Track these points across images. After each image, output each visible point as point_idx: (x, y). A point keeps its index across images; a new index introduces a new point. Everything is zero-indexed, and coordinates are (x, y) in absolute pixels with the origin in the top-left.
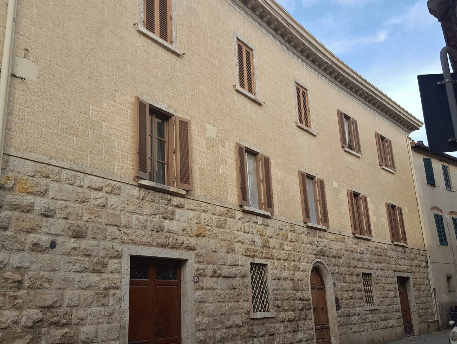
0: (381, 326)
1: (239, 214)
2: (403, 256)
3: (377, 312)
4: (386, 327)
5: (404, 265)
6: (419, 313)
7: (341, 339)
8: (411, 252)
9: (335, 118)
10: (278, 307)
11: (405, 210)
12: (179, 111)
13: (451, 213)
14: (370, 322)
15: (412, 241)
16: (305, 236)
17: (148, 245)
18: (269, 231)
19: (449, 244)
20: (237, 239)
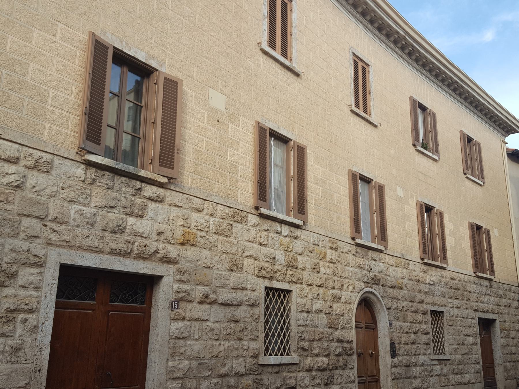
2: (489, 292)
3: (448, 362)
5: (489, 303)
6: (505, 367)
8: (499, 288)
11: (494, 234)
12: (437, 207)
14: (438, 375)
16: (351, 257)
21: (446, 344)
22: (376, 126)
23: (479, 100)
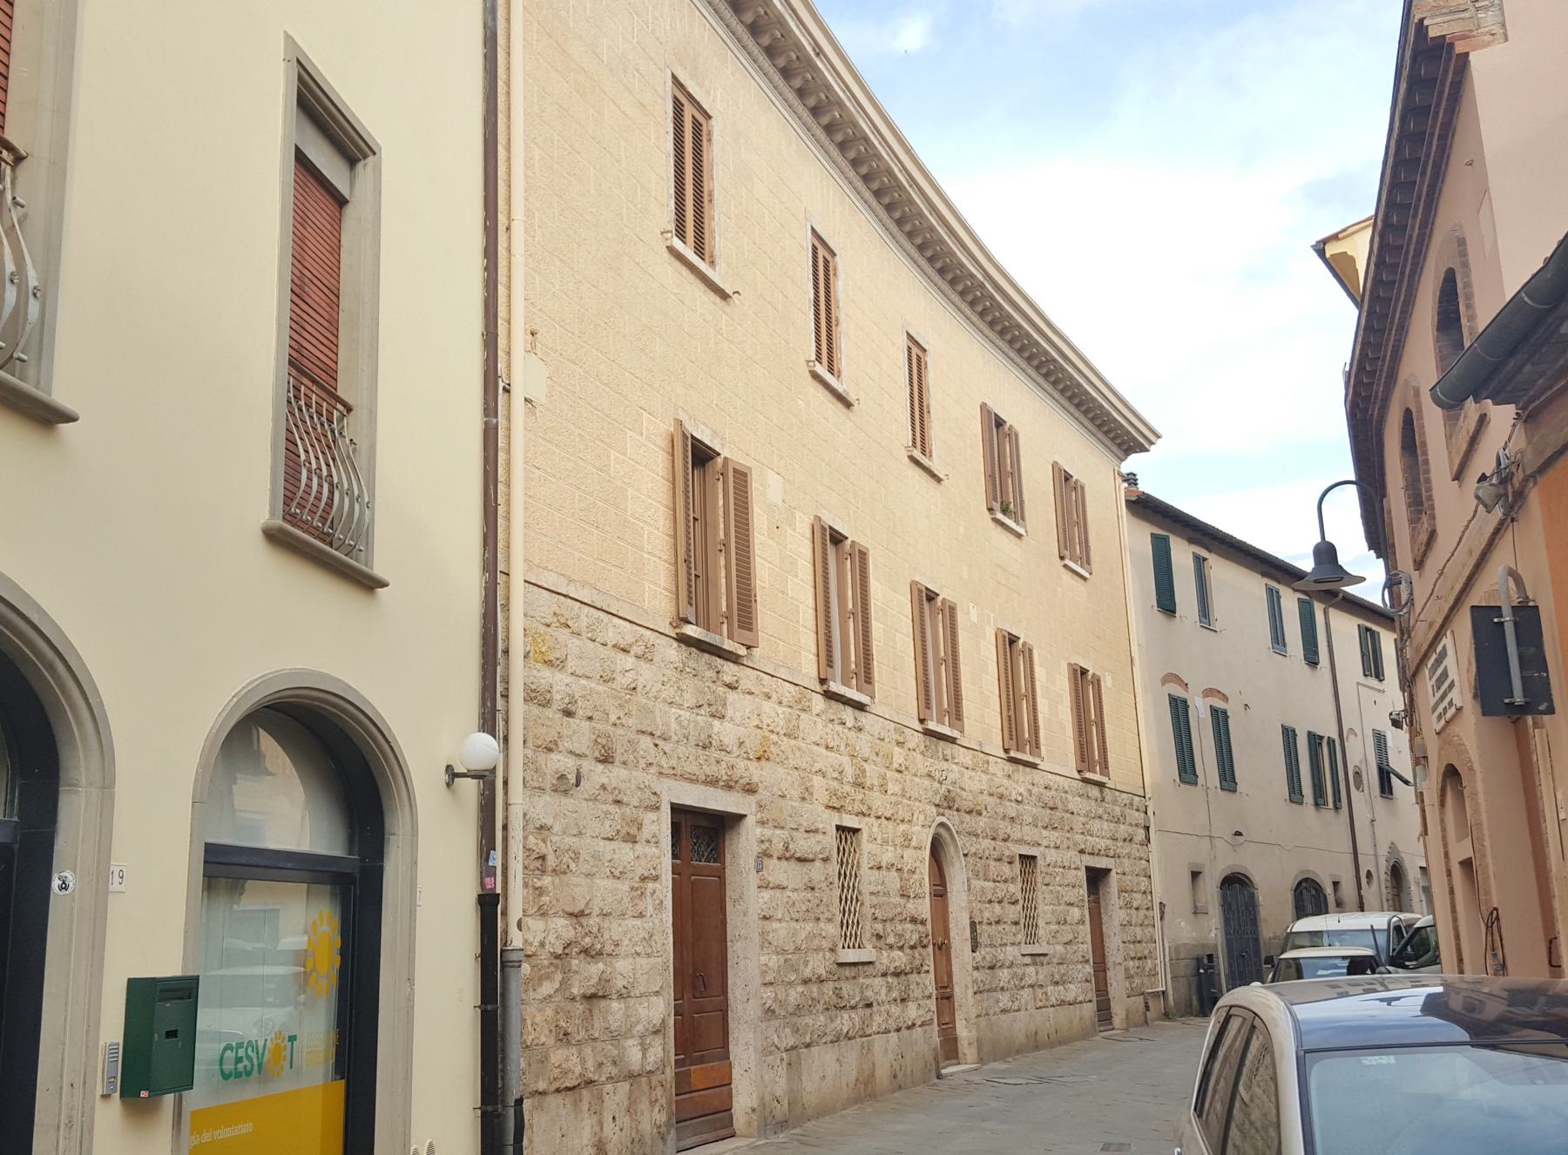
0: (1053, 1001)
1: (818, 702)
2: (1100, 811)
3: (1045, 960)
4: (1062, 1003)
5: (1100, 835)
6: (1127, 970)
7: (977, 1025)
8: (1115, 802)
9: (976, 427)
10: (879, 937)
11: (1107, 683)
12: (728, 449)
13: (1209, 693)
14: (1032, 986)
15: (1120, 773)
16: (919, 757)
17: (692, 781)
18: (863, 744)
19: (1201, 780)
20: (817, 766)
21: (1041, 923)
22: (939, 480)
23: (1087, 393)
